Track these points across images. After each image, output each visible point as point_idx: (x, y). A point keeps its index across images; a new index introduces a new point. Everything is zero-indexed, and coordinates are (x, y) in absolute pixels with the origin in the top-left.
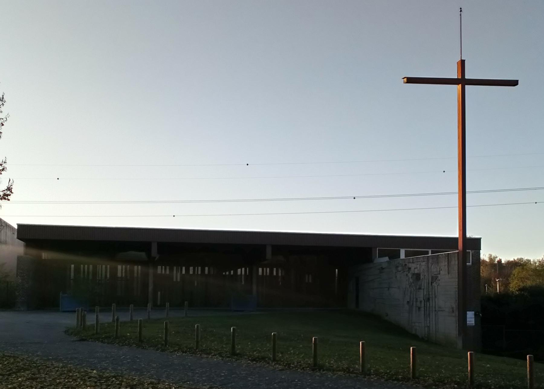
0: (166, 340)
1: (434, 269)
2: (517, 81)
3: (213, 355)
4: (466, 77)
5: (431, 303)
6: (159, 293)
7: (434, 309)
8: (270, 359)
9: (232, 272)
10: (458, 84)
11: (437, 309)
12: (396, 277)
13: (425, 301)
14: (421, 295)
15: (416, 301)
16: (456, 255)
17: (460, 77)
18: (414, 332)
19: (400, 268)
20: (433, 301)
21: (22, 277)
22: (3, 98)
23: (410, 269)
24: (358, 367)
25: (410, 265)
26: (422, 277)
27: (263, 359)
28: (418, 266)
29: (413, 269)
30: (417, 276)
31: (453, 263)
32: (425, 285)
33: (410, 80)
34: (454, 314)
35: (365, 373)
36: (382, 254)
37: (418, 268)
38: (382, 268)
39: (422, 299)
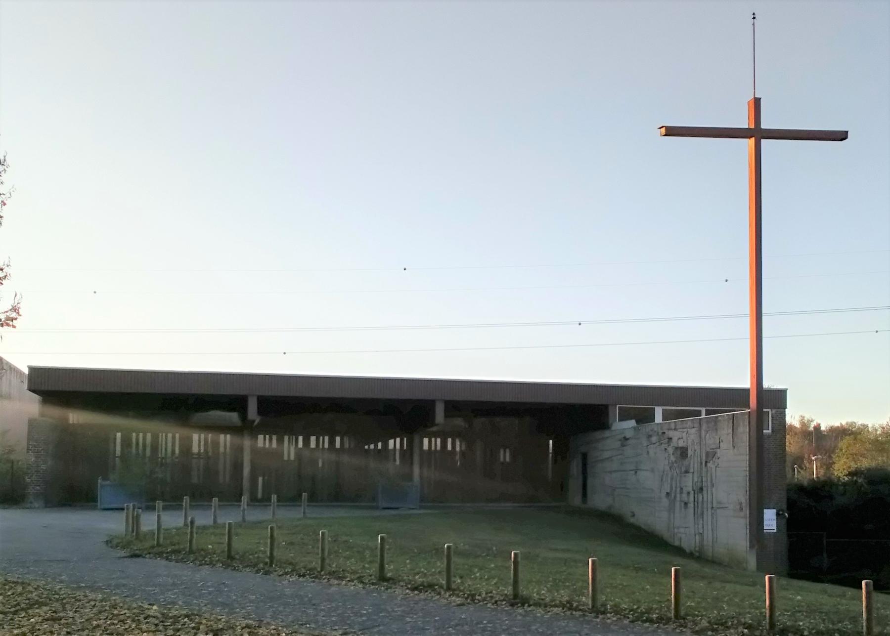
0: (271, 557)
1: (710, 440)
2: (847, 132)
3: (349, 581)
4: (763, 127)
5: (705, 496)
6: (260, 479)
7: (710, 506)
8: (441, 587)
12: (648, 452)
13: (696, 492)
14: (689, 483)
15: (681, 493)
17: (753, 127)
18: (677, 543)
19: (654, 439)
20: (709, 492)
21: (36, 452)
25: (671, 434)
26: (690, 452)
28: (684, 435)
29: (675, 439)
30: (683, 452)
33: (671, 132)
34: (742, 514)
37: (685, 438)
38: (626, 439)
39: (690, 489)
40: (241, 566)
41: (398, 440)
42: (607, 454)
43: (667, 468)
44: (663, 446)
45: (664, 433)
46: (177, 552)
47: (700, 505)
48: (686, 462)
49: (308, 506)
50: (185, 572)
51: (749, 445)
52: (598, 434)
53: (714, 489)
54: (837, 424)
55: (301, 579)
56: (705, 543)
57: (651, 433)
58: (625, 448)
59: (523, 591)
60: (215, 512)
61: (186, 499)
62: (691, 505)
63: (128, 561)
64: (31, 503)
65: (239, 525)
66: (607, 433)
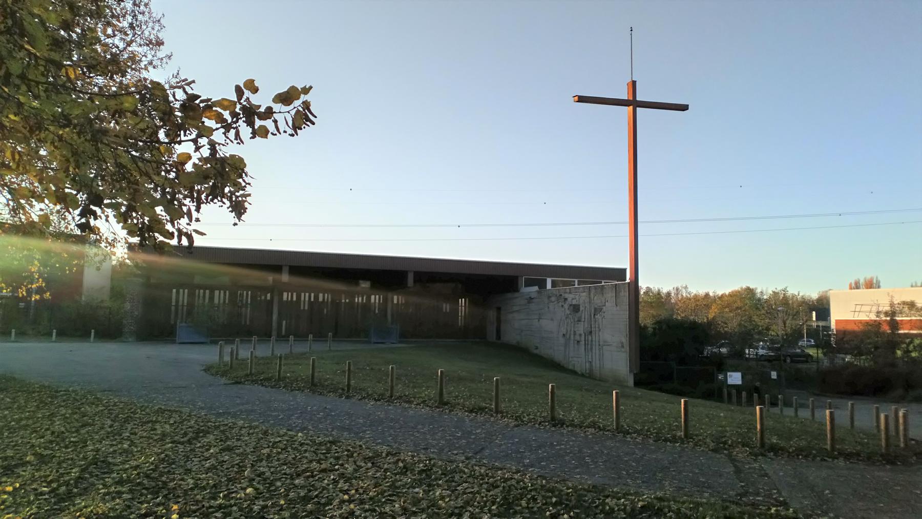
0: (349, 385)
1: (597, 300)
2: (688, 105)
3: (417, 405)
4: (638, 99)
5: (594, 337)
6: (284, 322)
7: (597, 344)
8: (491, 410)
9: (269, 295)
10: (629, 106)
11: (601, 344)
12: (548, 307)
13: (587, 334)
14: (581, 328)
15: (575, 334)
16: (627, 285)
17: (631, 99)
18: (571, 367)
19: (553, 299)
20: (597, 335)
22: (178, 74)
23: (566, 299)
24: (681, 434)
25: (566, 296)
26: (581, 308)
27: (482, 409)
28: (577, 297)
29: (569, 299)
30: (576, 308)
31: (622, 294)
32: (586, 317)
33: (582, 99)
34: (623, 350)
35: (619, 429)
36: (529, 283)
37: (577, 299)
38: (531, 298)
39: (582, 332)
40: (325, 392)
41: (377, 297)
42: (515, 308)
43: (564, 318)
44: (560, 304)
45: (561, 295)
46: (269, 379)
47: (590, 343)
48: (578, 315)
49: (333, 340)
50: (280, 399)
51: (629, 305)
52: (509, 295)
53: (601, 333)
54: (766, 287)
55: (378, 403)
56: (594, 368)
57: (551, 295)
58: (530, 304)
59: (560, 414)
60: (273, 346)
61: (311, 336)
62: (583, 343)
63: (234, 386)
64: (127, 338)
65: (287, 357)
66: (516, 295)
